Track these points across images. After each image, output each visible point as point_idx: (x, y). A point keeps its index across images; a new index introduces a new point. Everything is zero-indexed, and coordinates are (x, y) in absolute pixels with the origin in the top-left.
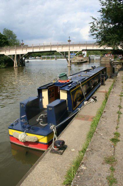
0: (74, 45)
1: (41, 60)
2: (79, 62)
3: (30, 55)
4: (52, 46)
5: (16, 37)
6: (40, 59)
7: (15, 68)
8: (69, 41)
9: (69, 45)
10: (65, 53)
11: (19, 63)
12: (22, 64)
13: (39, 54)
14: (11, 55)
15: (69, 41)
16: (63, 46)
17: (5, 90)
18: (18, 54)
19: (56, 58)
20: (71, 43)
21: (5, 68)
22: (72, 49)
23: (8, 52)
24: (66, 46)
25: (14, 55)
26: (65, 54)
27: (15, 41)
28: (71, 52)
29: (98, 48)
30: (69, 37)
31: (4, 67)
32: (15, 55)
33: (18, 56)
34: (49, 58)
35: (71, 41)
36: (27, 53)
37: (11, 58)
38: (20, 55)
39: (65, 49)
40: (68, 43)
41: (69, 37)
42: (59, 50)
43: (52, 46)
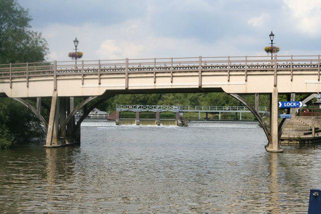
0: (293, 69)
1: (114, 124)
2: (308, 140)
3: (105, 102)
4: (205, 69)
5: (24, 22)
6: (110, 120)
7: (48, 151)
8: (271, 50)
9: (274, 69)
10: (257, 98)
11: (63, 133)
12: (71, 136)
13: (145, 105)
14: (34, 99)
15: (271, 50)
16: (249, 70)
17: (280, 196)
18: (62, 93)
19: (181, 118)
20: (283, 56)
21: (11, 147)
22: (286, 84)
23: (20, 89)
24: (263, 70)
25: (45, 102)
26: (252, 108)
27: (21, 35)
28: (287, 96)
29: (238, 98)
30: (272, 35)
31: (9, 143)
32: (51, 98)
33: (64, 102)
34: (168, 117)
35: (277, 50)
36: (100, 92)
37: (33, 110)
38: (72, 100)
39: (260, 84)
40: (265, 58)
41: (272, 35)
42: (234, 85)
43: (205, 69)
